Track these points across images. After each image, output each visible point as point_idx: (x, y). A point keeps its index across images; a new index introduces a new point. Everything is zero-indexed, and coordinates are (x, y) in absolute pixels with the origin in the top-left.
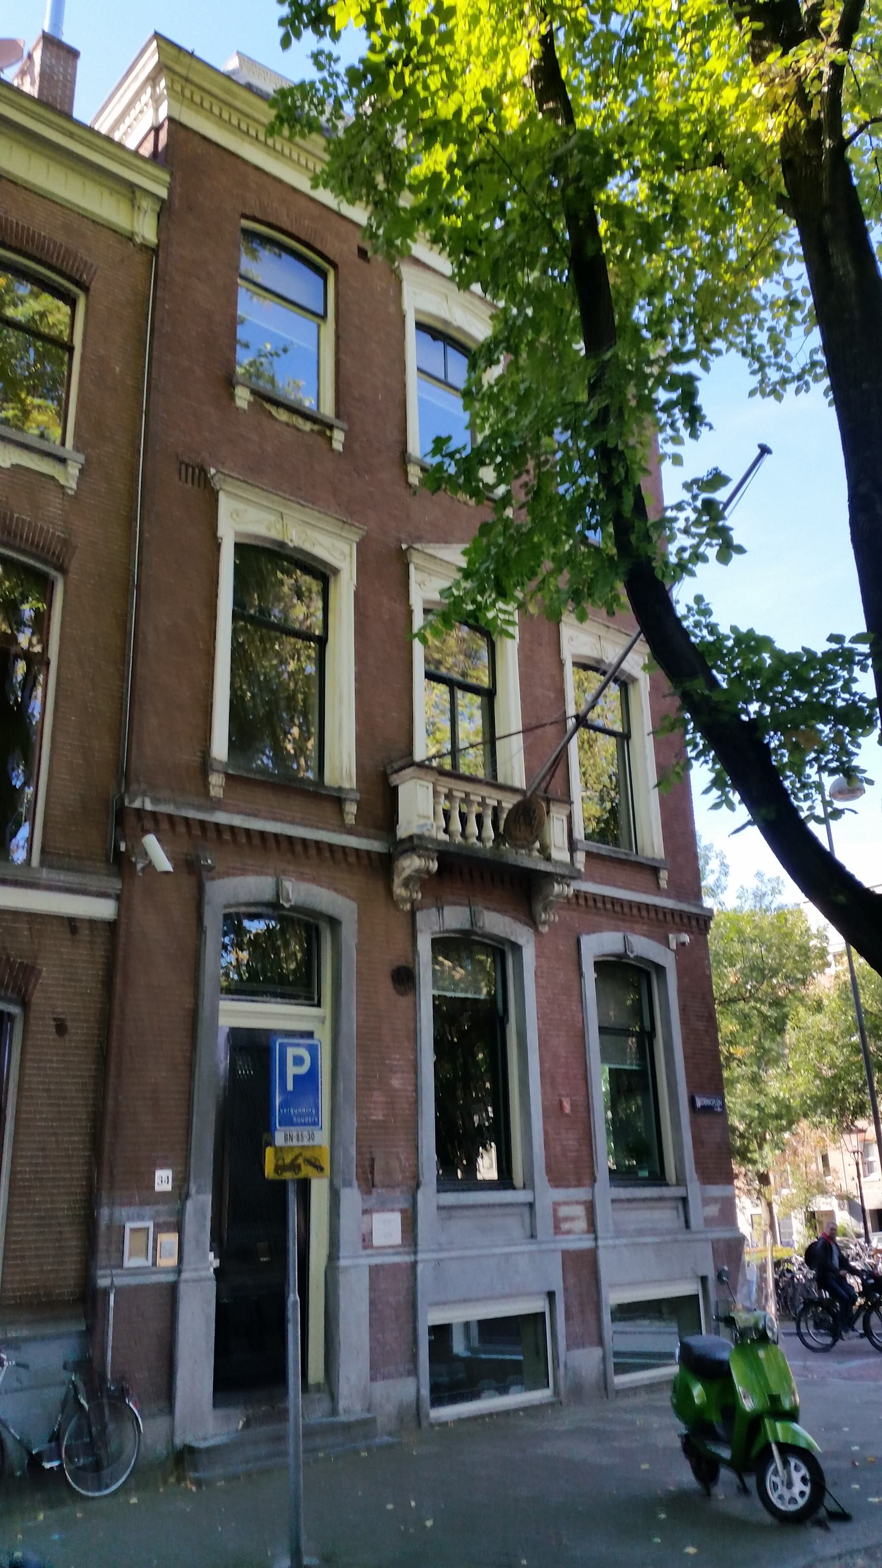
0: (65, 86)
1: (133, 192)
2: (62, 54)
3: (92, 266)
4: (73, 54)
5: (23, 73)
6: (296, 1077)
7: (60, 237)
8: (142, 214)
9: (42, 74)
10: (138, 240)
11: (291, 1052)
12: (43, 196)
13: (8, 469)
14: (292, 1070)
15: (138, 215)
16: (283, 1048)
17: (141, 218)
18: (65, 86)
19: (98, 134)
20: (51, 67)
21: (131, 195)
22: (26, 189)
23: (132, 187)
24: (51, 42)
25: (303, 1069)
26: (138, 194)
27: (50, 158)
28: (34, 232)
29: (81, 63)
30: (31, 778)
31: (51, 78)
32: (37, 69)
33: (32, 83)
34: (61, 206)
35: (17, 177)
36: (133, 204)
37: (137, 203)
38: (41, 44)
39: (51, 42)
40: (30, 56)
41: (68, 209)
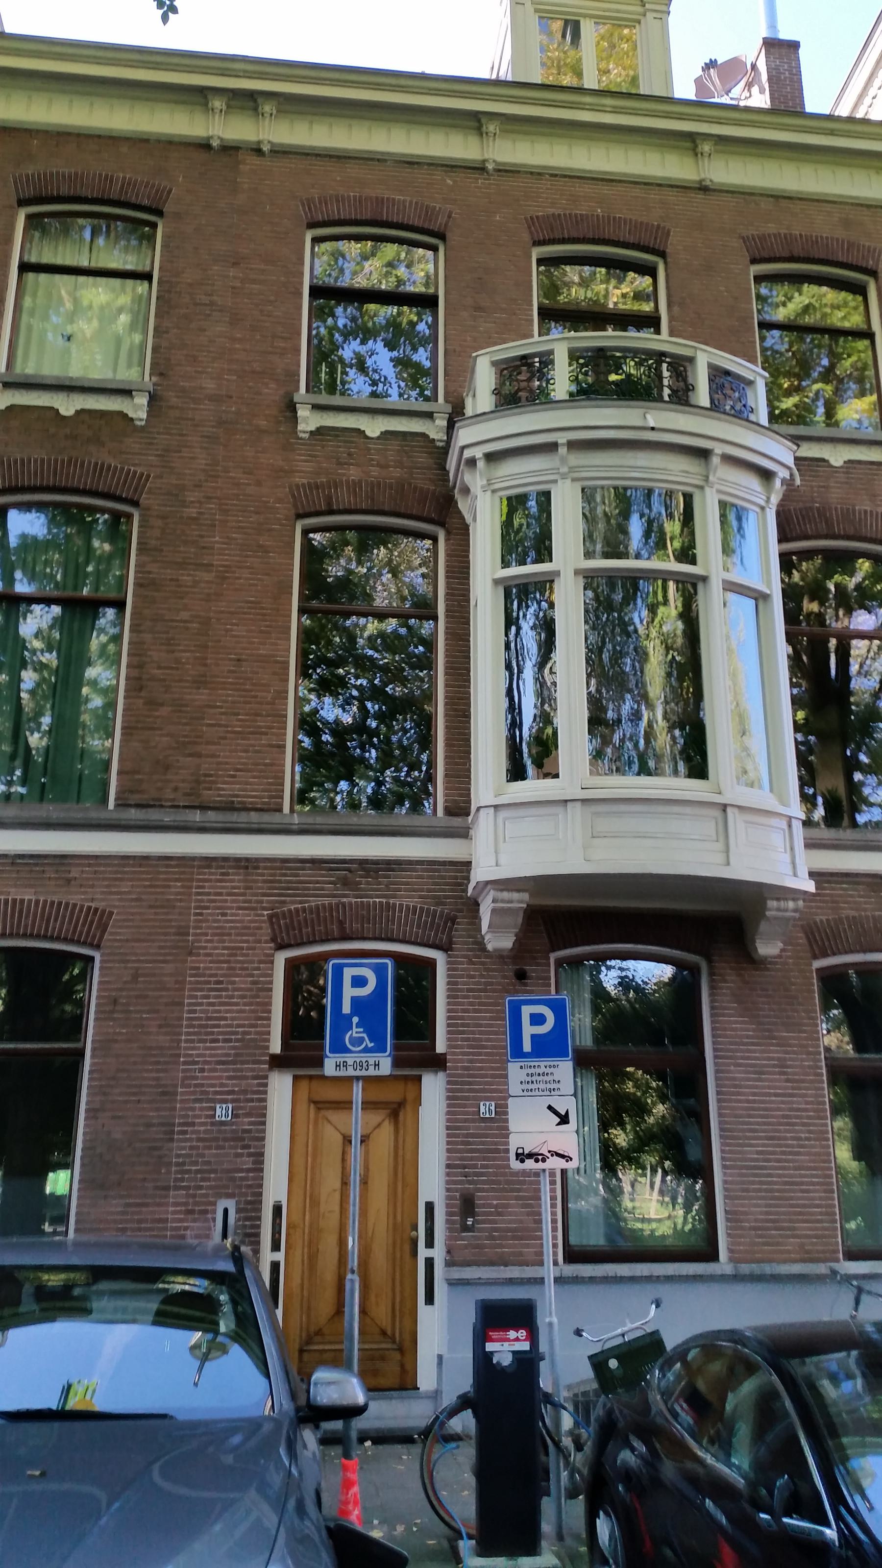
0: (791, 80)
1: (479, 121)
2: (784, 51)
3: (875, 250)
4: (794, 46)
5: (749, 85)
6: (355, 1000)
7: (840, 233)
8: (706, 160)
9: (770, 79)
10: (215, 143)
11: (348, 973)
12: (818, 201)
13: (841, 467)
14: (349, 992)
15: (214, 116)
16: (338, 972)
17: (491, 144)
18: (791, 80)
19: (839, 119)
20: (777, 68)
21: (477, 124)
22: (801, 199)
23: (692, 138)
24: (772, 45)
25: (364, 992)
26: (256, 96)
27: (661, 146)
28: (817, 237)
29: (801, 51)
30: (297, 743)
31: (779, 79)
32: (764, 77)
33: (762, 91)
34: (834, 202)
35: (791, 191)
36: (695, 153)
37: (699, 149)
38: (763, 51)
39: (772, 45)
40: (754, 66)
41: (841, 203)
